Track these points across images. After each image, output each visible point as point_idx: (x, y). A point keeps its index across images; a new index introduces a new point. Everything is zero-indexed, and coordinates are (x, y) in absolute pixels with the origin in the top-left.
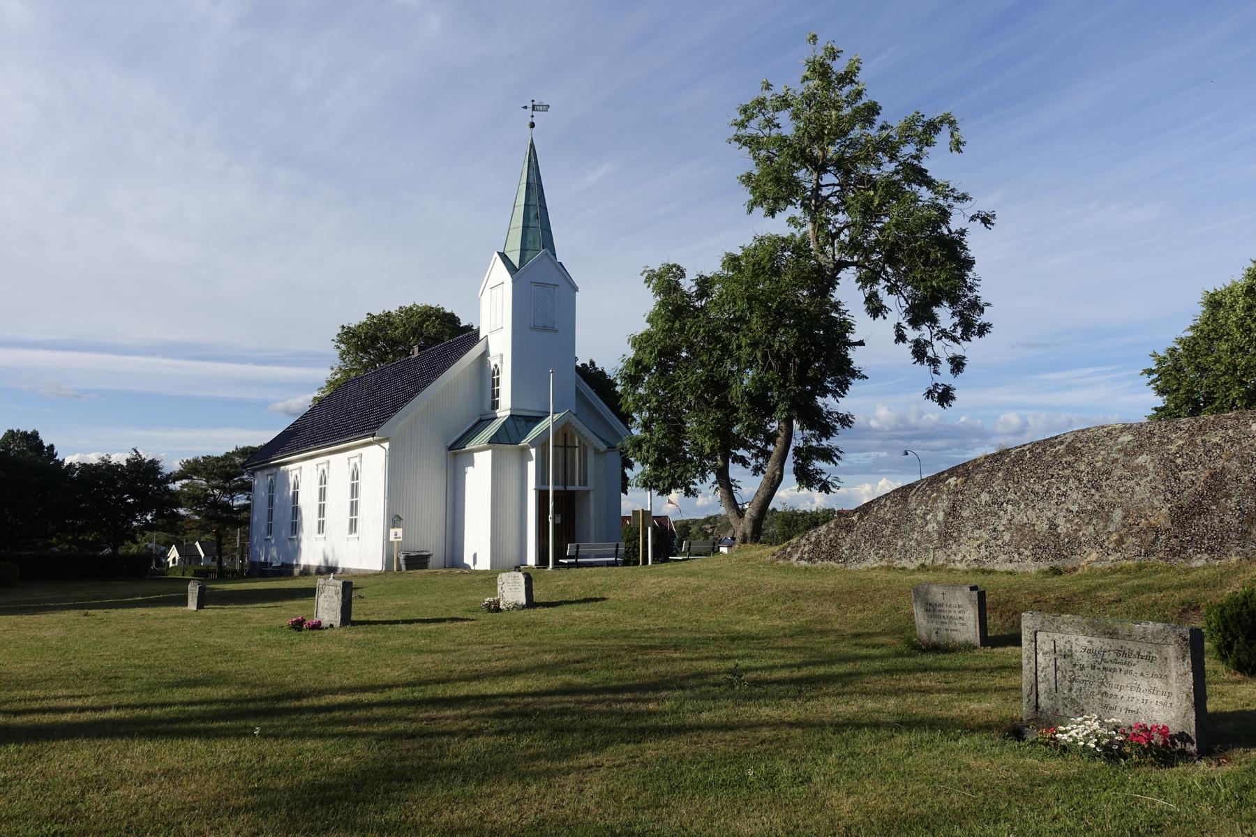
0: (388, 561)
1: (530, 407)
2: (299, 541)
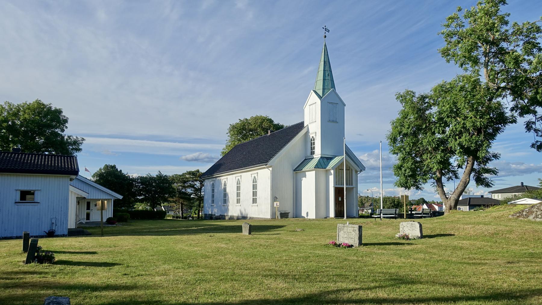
0: (273, 214)
1: (329, 154)
2: (228, 206)
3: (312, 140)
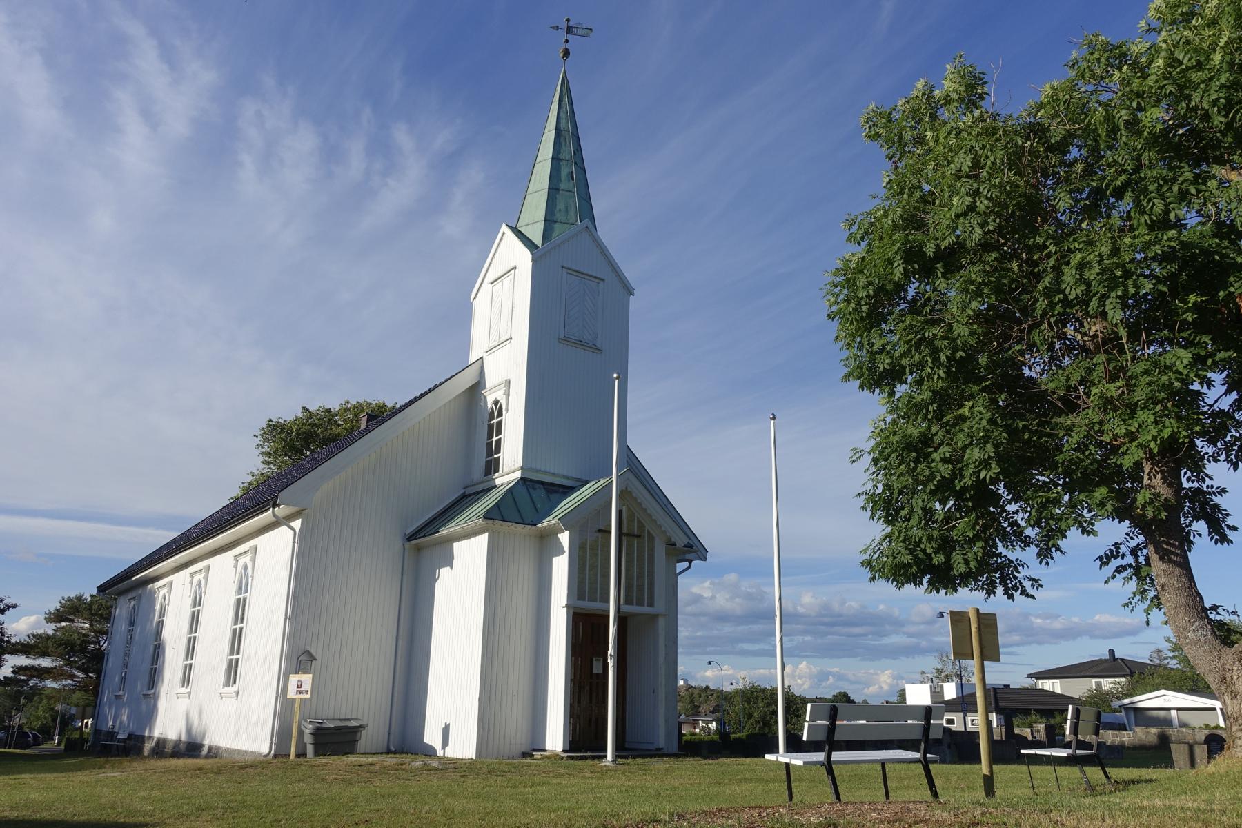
0: (282, 736)
1: (556, 468)
2: (156, 697)
3: (491, 417)
